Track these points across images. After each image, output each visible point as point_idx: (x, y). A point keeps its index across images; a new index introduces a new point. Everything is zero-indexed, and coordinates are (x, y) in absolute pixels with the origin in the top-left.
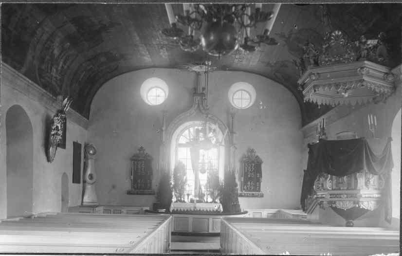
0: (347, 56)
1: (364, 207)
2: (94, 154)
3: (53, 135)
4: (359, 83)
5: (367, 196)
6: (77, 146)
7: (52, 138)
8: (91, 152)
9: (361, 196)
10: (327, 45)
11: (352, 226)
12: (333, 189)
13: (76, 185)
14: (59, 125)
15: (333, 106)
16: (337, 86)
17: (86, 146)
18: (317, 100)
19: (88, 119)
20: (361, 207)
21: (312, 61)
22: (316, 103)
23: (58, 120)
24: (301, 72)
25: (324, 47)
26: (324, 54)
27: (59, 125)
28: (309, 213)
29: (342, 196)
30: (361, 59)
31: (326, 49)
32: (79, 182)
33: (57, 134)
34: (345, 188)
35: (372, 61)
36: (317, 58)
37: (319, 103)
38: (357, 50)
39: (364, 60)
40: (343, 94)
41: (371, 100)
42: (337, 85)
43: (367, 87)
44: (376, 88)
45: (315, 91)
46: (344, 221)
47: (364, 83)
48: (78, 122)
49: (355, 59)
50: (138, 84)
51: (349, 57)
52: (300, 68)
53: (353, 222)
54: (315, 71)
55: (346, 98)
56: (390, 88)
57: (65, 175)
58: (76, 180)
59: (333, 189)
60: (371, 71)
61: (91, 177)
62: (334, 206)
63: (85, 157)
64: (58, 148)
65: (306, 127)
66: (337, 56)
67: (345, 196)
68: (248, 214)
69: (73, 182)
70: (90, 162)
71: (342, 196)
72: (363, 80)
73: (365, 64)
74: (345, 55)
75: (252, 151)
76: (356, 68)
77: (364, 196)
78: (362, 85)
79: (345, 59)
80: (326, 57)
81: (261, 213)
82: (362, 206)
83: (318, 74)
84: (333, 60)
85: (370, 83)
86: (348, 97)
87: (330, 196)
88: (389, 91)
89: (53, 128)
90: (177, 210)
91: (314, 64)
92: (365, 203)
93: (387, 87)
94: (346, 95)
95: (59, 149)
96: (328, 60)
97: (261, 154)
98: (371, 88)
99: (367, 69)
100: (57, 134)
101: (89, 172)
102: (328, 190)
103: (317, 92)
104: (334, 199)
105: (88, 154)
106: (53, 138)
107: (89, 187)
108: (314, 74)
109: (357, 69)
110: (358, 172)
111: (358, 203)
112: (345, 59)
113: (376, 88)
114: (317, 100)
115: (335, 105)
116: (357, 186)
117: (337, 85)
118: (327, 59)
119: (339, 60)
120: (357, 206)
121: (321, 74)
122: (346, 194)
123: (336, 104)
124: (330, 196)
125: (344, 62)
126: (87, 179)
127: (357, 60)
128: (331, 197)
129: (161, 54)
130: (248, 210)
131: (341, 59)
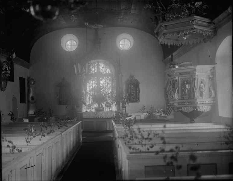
0: (183, 13)
1: (200, 110)
2: (33, 84)
3: (4, 74)
4: (192, 30)
5: (201, 103)
6: (22, 80)
7: (3, 76)
8: (32, 83)
9: (197, 103)
10: (170, 7)
11: (194, 123)
12: (179, 100)
13: (23, 104)
14: (7, 67)
15: (178, 46)
16: (178, 33)
17: (28, 78)
18: (167, 43)
19: (29, 62)
20: (198, 110)
21: (161, 19)
22: (167, 44)
23: (6, 64)
24: (156, 25)
25: (168, 8)
26: (168, 13)
27: (7, 67)
28: (168, 115)
29: (185, 104)
30: (192, 15)
31: (170, 10)
32: (24, 102)
33: (6, 73)
34: (187, 98)
35: (200, 16)
36: (164, 16)
37: (169, 44)
38: (189, 9)
39: (194, 15)
40: (183, 37)
41: (202, 41)
42: (178, 33)
43: (197, 32)
44: (203, 32)
45: (164, 37)
46: (188, 119)
47: (195, 30)
48: (22, 65)
49: (188, 15)
50: (60, 37)
51: (184, 14)
52: (155, 22)
53: (194, 120)
54: (164, 24)
55: (185, 40)
56: (213, 32)
57: (14, 99)
58: (23, 100)
59: (179, 100)
60: (199, 22)
61: (33, 98)
62: (180, 110)
63: (28, 86)
64: (8, 82)
65: (166, 59)
66: (177, 13)
67: (187, 103)
68: (132, 116)
69: (21, 103)
70: (31, 89)
71: (185, 104)
72: (194, 28)
73: (194, 17)
74: (182, 13)
75: (132, 77)
76: (189, 20)
77: (199, 103)
78: (194, 32)
79: (182, 15)
80: (170, 15)
81: (140, 116)
82: (199, 110)
83: (165, 26)
84: (174, 16)
85: (199, 30)
86: (186, 39)
87: (178, 104)
88: (212, 34)
89: (3, 69)
90: (101, 118)
91: (162, 20)
92: (201, 108)
93: (210, 31)
94: (185, 38)
95: (9, 83)
96: (171, 17)
97: (139, 77)
98: (200, 33)
99: (196, 21)
100: (6, 73)
101: (31, 95)
102: (176, 100)
103: (165, 37)
104: (180, 106)
105: (31, 85)
106: (4, 76)
107: (31, 105)
108: (163, 26)
109: (190, 21)
110: (83, 90)
111: (196, 107)
112: (182, 15)
113: (203, 32)
114: (167, 43)
115: (179, 45)
116: (194, 97)
117: (178, 33)
118: (170, 16)
119: (178, 16)
120: (196, 109)
121: (168, 26)
122: (187, 102)
123: (180, 44)
124: (178, 104)
125: (182, 17)
126: (30, 99)
127: (190, 15)
128: (178, 105)
129: (72, 18)
130: (131, 114)
131: (179, 15)
